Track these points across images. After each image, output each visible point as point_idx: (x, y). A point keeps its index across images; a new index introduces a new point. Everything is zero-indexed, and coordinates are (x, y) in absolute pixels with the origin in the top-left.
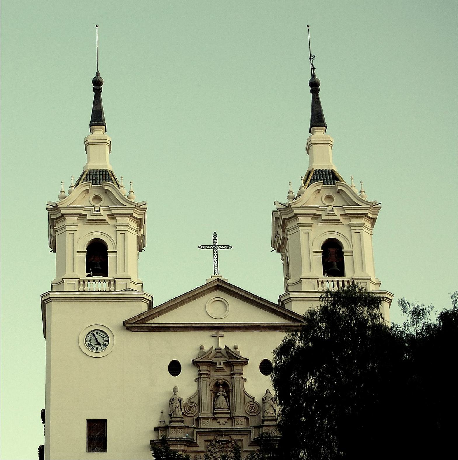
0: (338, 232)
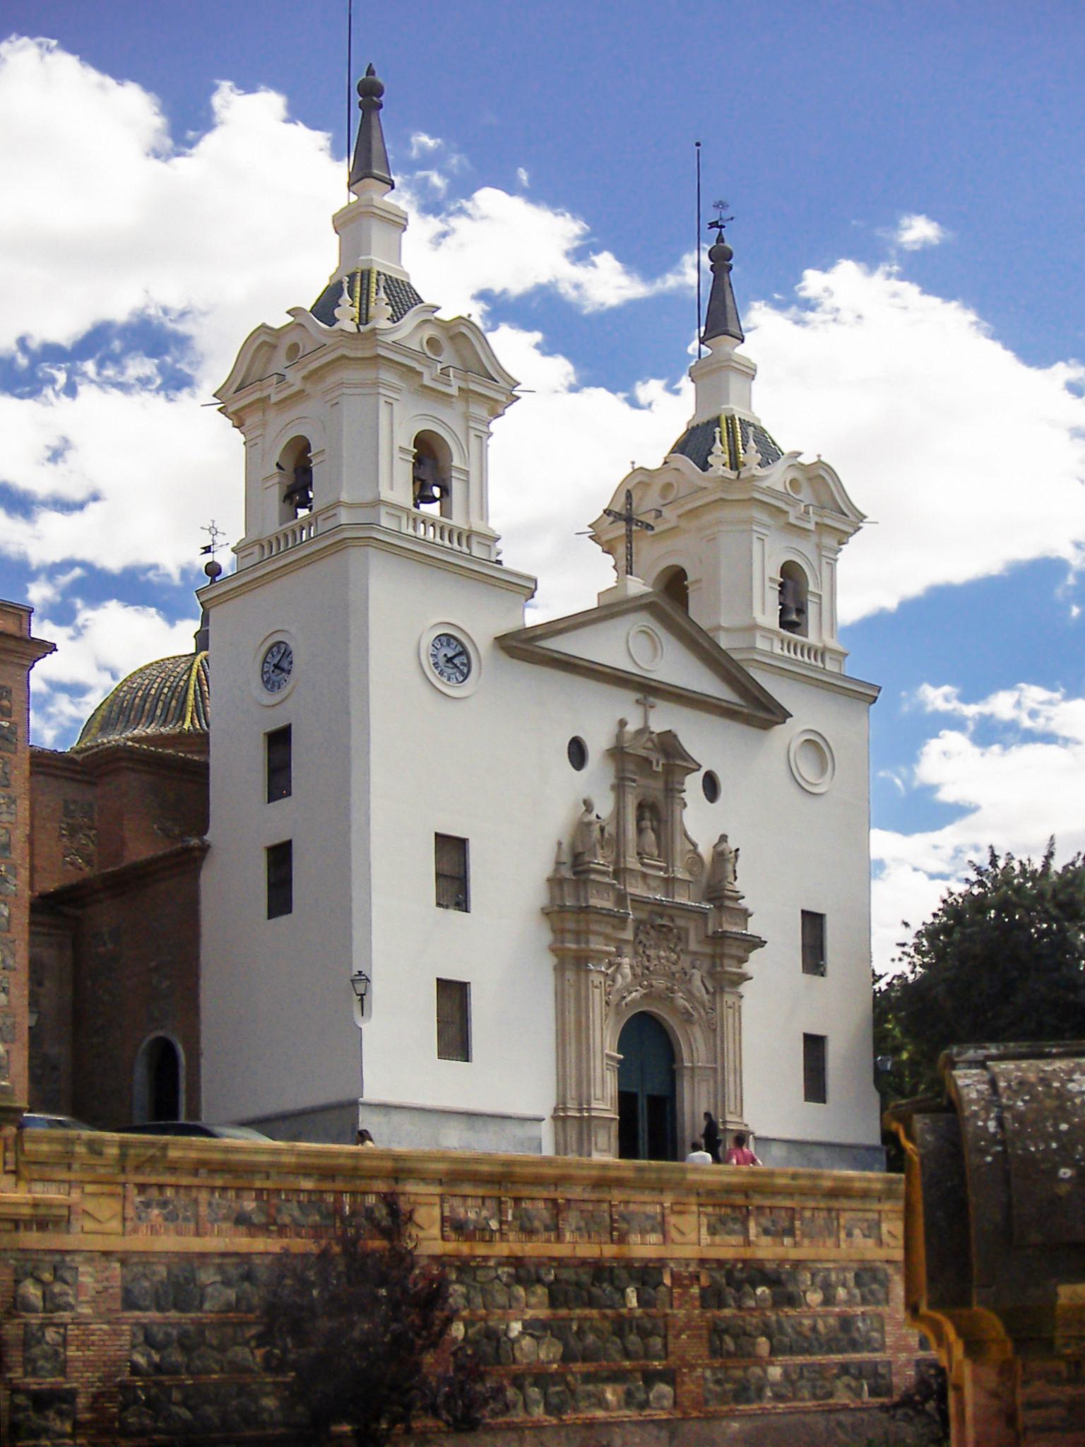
0: (803, 553)
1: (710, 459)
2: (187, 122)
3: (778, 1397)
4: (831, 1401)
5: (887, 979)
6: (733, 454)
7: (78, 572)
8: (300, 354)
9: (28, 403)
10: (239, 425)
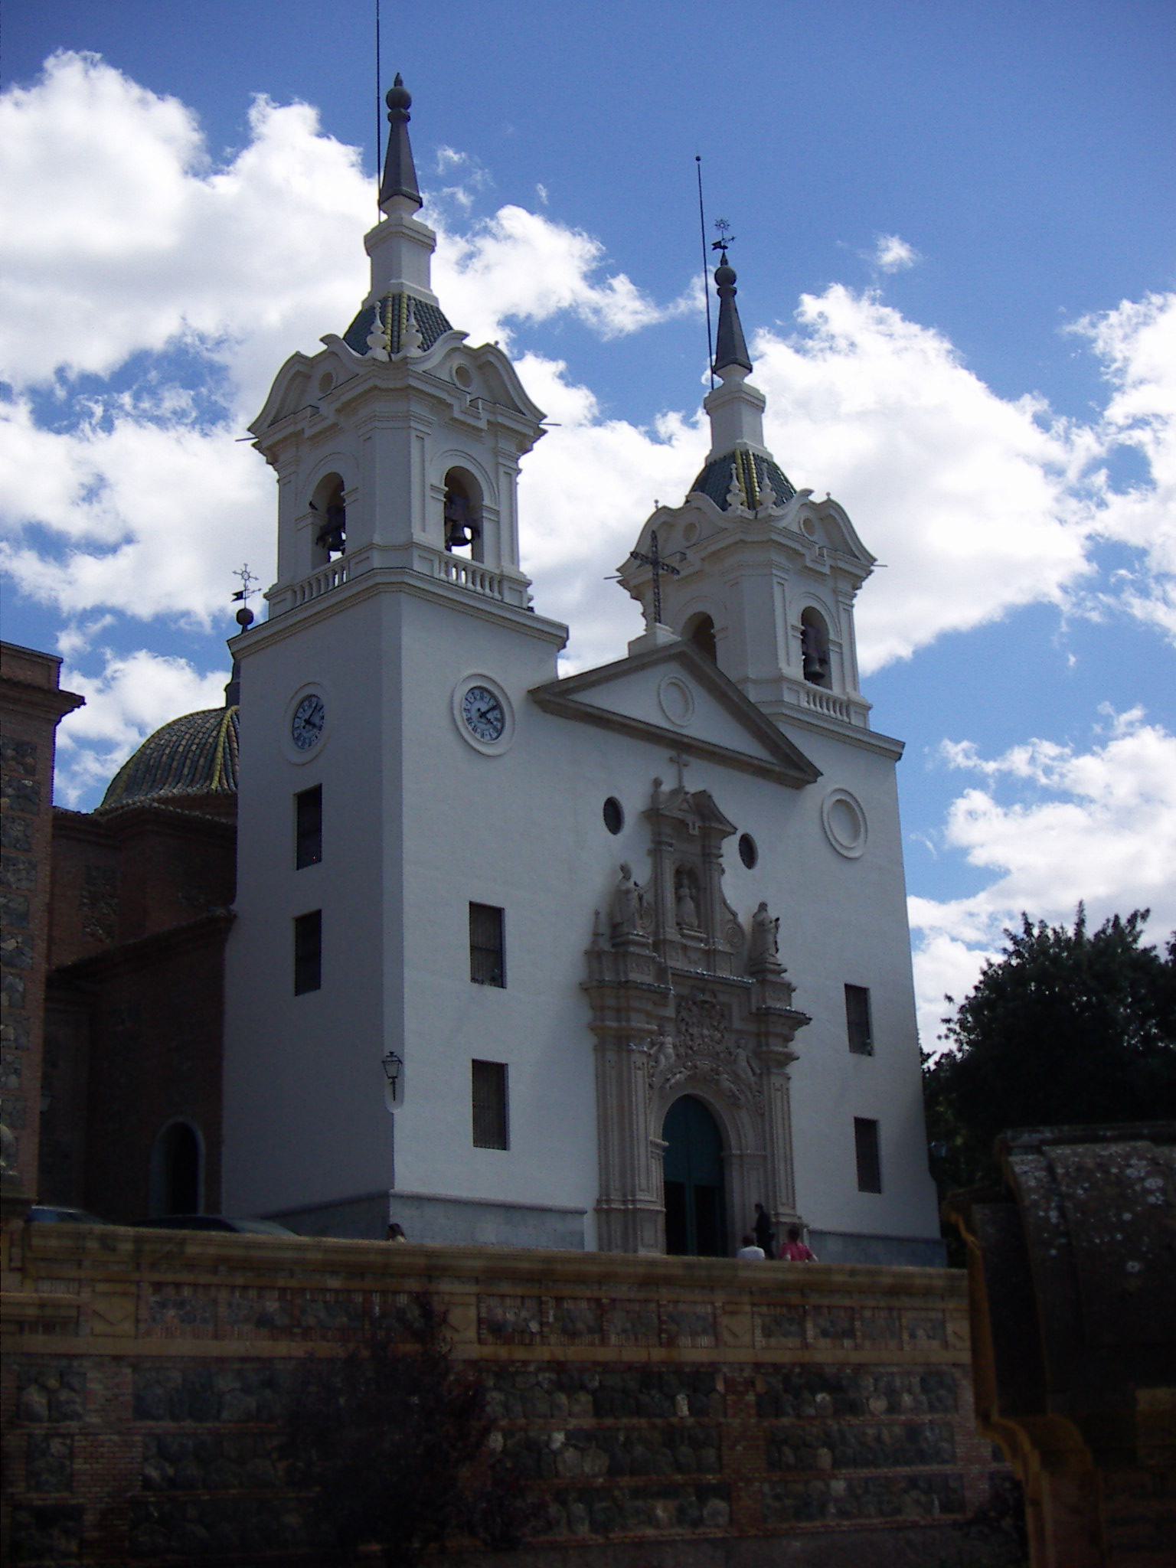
1: (729, 498)
2: (223, 139)
3: (843, 1514)
4: (899, 1518)
5: (936, 1057)
6: (750, 491)
7: (108, 619)
8: (333, 385)
9: (64, 439)
10: (272, 461)
